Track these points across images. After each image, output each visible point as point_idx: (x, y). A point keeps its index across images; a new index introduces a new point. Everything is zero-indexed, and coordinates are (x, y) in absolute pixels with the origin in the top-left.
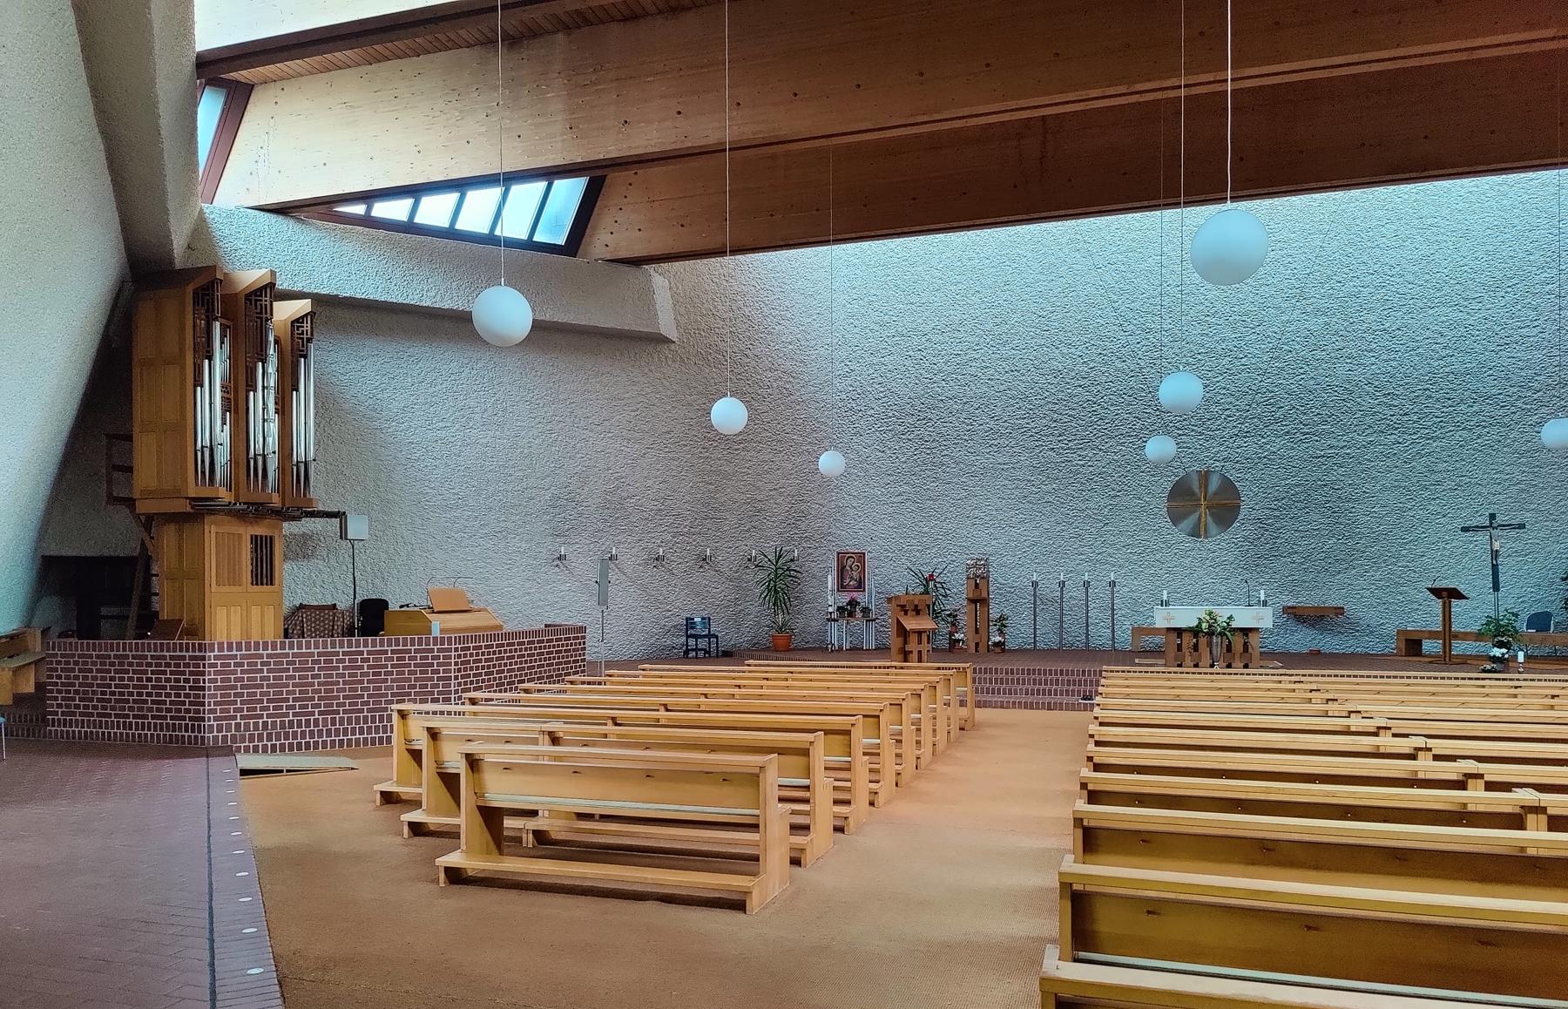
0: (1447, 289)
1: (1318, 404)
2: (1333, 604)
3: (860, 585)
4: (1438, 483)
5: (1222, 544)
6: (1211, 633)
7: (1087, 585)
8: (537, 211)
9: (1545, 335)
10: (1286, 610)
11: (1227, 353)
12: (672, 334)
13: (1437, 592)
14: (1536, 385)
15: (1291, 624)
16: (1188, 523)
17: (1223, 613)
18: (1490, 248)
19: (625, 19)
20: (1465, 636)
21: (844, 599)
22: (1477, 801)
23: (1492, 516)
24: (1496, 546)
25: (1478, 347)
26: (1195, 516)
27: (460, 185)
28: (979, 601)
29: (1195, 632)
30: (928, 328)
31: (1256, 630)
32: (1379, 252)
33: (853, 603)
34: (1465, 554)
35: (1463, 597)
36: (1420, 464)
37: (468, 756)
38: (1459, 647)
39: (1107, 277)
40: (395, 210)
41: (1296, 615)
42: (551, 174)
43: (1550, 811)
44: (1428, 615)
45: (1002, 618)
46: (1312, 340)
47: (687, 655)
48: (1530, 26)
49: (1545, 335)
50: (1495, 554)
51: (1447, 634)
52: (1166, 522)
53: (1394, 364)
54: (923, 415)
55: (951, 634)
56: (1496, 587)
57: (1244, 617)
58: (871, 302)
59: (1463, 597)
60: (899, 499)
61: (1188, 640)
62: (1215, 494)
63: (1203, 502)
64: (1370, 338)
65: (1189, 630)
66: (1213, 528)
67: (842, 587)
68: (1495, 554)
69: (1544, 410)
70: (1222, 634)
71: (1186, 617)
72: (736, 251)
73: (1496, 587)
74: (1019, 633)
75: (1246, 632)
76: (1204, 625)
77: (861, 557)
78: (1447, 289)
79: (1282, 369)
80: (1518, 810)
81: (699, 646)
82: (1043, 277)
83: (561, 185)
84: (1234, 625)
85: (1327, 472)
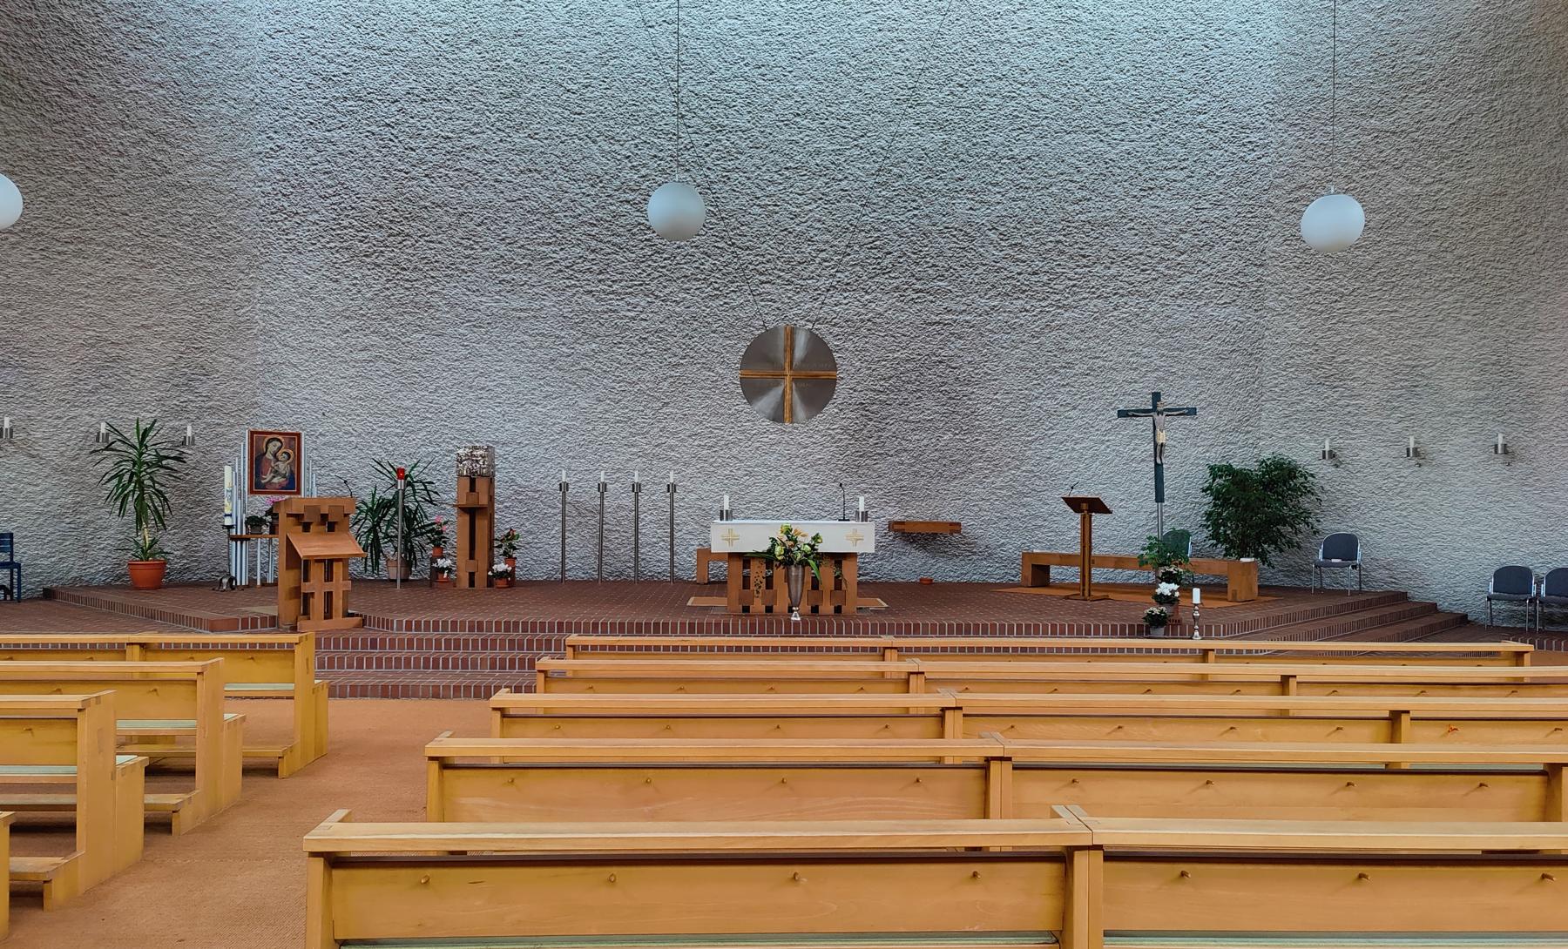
0: (1086, 110)
1: (933, 252)
2: (948, 519)
3: (292, 484)
4: (1069, 366)
5: (816, 434)
6: (788, 562)
7: (637, 488)
9: (1193, 181)
10: (893, 525)
11: (822, 171)
13: (1074, 503)
14: (1180, 244)
15: (899, 545)
16: (768, 402)
17: (806, 530)
18: (1138, 58)
20: (1104, 561)
21: (261, 504)
23: (1156, 396)
24: (1162, 438)
25: (1119, 191)
26: (780, 390)
28: (476, 512)
29: (768, 558)
30: (400, 91)
31: (853, 555)
32: (1008, 50)
34: (1095, 457)
35: (1108, 511)
36: (1048, 340)
37: (788, 532)
38: (1099, 575)
41: (907, 534)
44: (1065, 532)
45: (510, 536)
46: (927, 163)
49: (1193, 181)
50: (1159, 449)
51: (1086, 559)
52: (741, 403)
53: (1023, 204)
54: (396, 229)
55: (433, 560)
56: (1160, 498)
57: (836, 537)
58: (304, 39)
59: (1108, 511)
60: (365, 355)
61: (757, 571)
62: (804, 361)
63: (790, 374)
64: (995, 167)
65: (756, 556)
66: (800, 412)
67: (257, 487)
68: (1159, 449)
69: (1187, 278)
70: (803, 564)
71: (754, 536)
73: (1160, 498)
74: (538, 556)
75: (838, 558)
76: (778, 550)
78: (1086, 110)
79: (891, 200)
82: (570, 31)
84: (821, 548)
85: (944, 342)
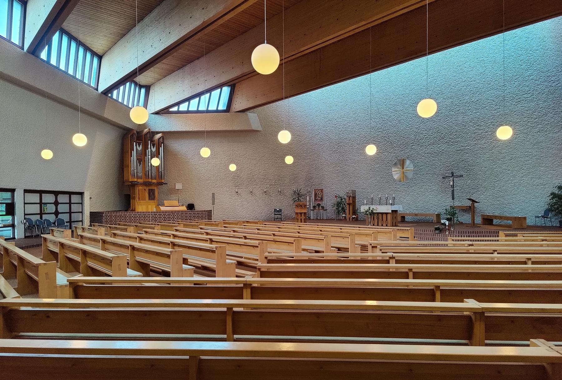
0: (492, 83)
3: (322, 199)
8: (218, 99)
12: (260, 129)
19: (242, 33)
22: (393, 268)
27: (188, 99)
32: (465, 73)
33: (319, 205)
39: (382, 95)
40: (175, 109)
42: (220, 86)
43: (413, 270)
47: (275, 220)
48: (357, 22)
67: (316, 200)
69: (540, 126)
72: (286, 98)
77: (322, 190)
80: (407, 270)
81: (278, 216)
83: (216, 93)
